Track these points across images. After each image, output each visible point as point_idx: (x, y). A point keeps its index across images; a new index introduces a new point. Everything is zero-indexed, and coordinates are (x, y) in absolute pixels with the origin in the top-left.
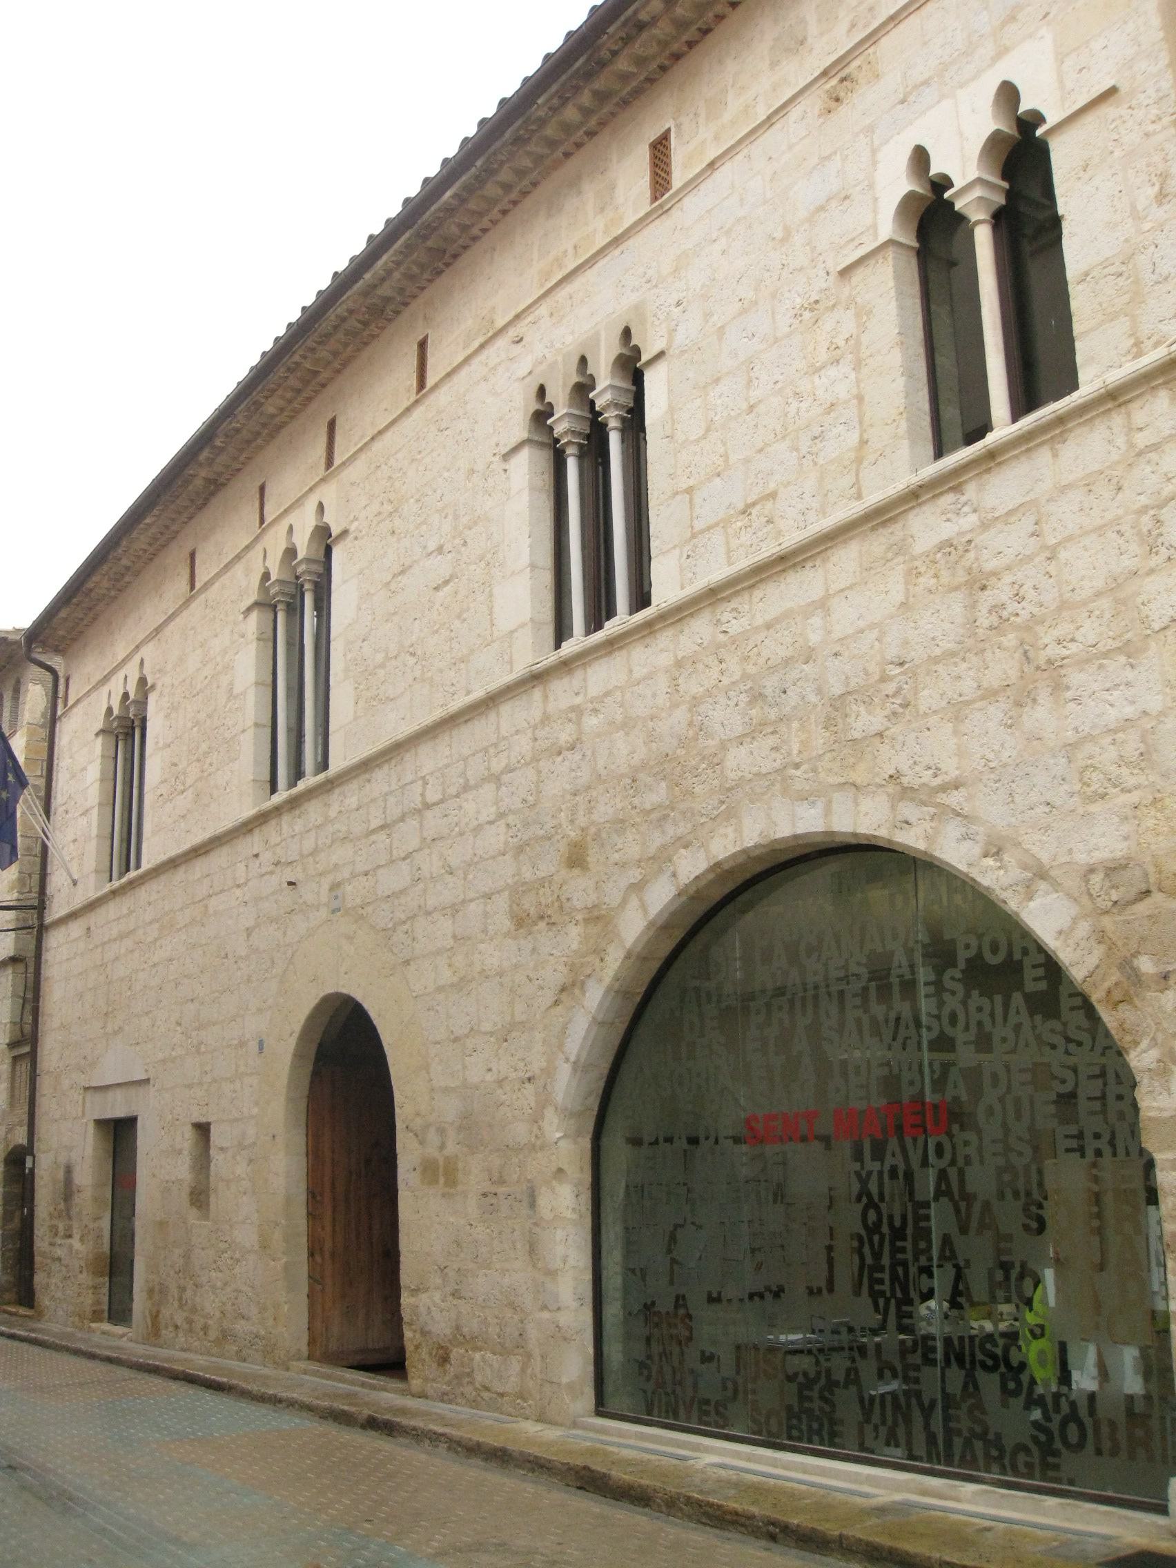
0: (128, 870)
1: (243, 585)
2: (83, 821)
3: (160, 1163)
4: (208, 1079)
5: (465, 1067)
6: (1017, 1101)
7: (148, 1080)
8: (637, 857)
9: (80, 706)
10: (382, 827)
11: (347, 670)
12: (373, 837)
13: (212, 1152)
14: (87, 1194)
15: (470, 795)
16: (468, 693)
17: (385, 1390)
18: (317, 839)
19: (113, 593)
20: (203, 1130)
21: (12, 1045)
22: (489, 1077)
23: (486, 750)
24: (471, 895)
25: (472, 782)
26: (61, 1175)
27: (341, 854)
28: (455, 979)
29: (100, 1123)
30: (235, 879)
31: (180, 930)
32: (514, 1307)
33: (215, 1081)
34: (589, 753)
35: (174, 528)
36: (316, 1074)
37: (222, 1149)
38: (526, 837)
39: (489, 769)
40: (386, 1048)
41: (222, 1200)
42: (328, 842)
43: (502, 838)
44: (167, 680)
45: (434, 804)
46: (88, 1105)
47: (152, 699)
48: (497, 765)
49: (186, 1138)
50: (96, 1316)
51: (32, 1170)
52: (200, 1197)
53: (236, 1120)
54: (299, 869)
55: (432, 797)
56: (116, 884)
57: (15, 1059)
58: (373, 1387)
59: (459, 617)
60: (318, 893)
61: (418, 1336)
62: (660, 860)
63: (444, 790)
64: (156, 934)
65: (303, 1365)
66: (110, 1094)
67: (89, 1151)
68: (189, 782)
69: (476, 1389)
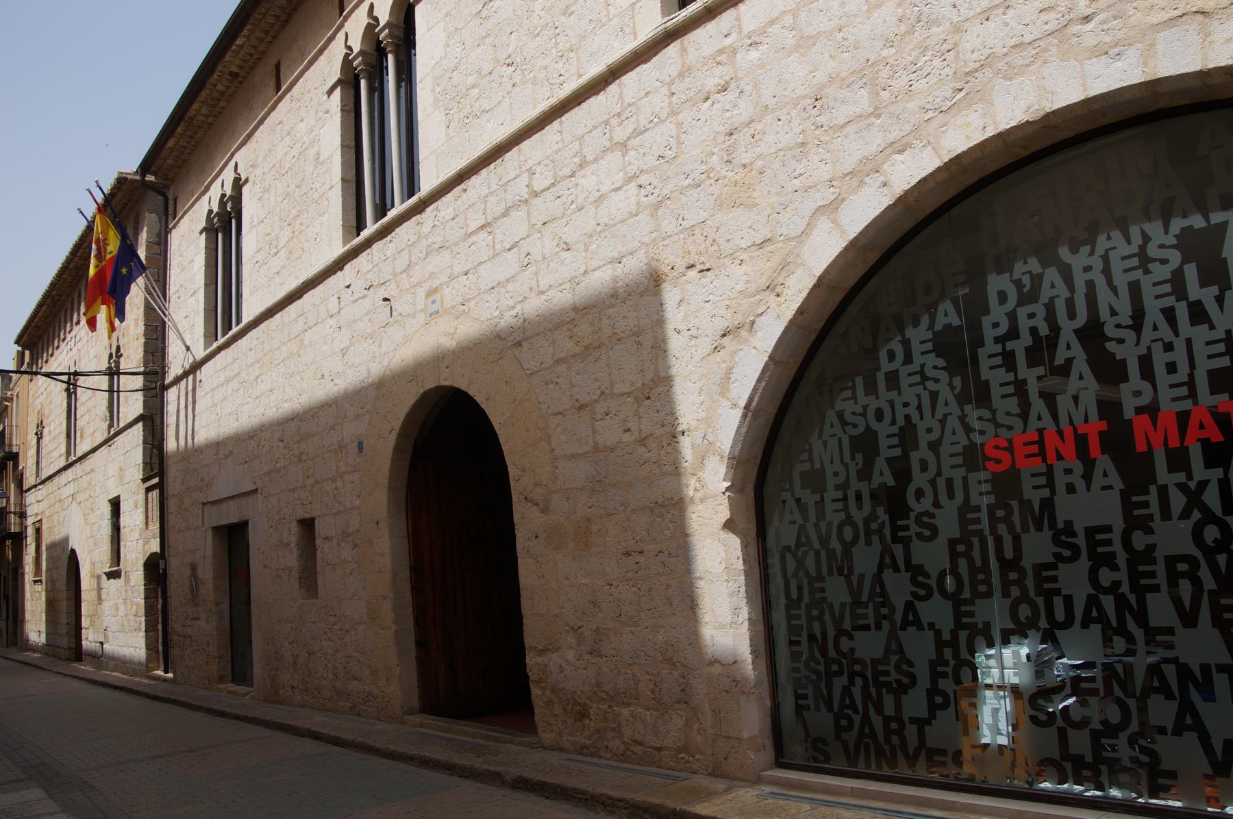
0: (230, 329)
1: (328, 67)
2: (192, 301)
3: (271, 553)
4: (311, 481)
5: (594, 431)
6: (950, 482)
7: (256, 491)
8: (827, 177)
9: (186, 217)
10: (483, 227)
11: (436, 101)
12: (473, 239)
13: (318, 542)
14: (210, 585)
15: (588, 171)
16: (580, 76)
17: (512, 743)
18: (410, 256)
19: (210, 120)
20: (308, 525)
21: (144, 480)
22: (626, 438)
23: (606, 123)
24: (594, 264)
25: (589, 158)
26: (188, 571)
27: (437, 262)
28: (578, 349)
29: (216, 529)
30: (328, 311)
31: (278, 365)
32: (671, 662)
33: (317, 482)
34: (748, 89)
35: (261, 48)
36: (413, 468)
37: (326, 538)
38: (665, 192)
39: (611, 139)
40: (496, 427)
41: (327, 580)
42: (423, 256)
43: (633, 200)
44: (259, 171)
45: (543, 191)
46: (206, 516)
47: (246, 191)
48: (620, 134)
49: (292, 533)
50: (221, 679)
51: (165, 570)
52: (309, 579)
53: (339, 512)
54: (393, 285)
55: (538, 185)
56: (221, 341)
57: (148, 490)
58: (498, 740)
59: (564, 13)
60: (414, 304)
61: (548, 693)
62: (871, 166)
63: (555, 173)
64: (257, 372)
65: (419, 719)
66: (224, 506)
67: (209, 551)
68: (281, 244)
69: (623, 743)
